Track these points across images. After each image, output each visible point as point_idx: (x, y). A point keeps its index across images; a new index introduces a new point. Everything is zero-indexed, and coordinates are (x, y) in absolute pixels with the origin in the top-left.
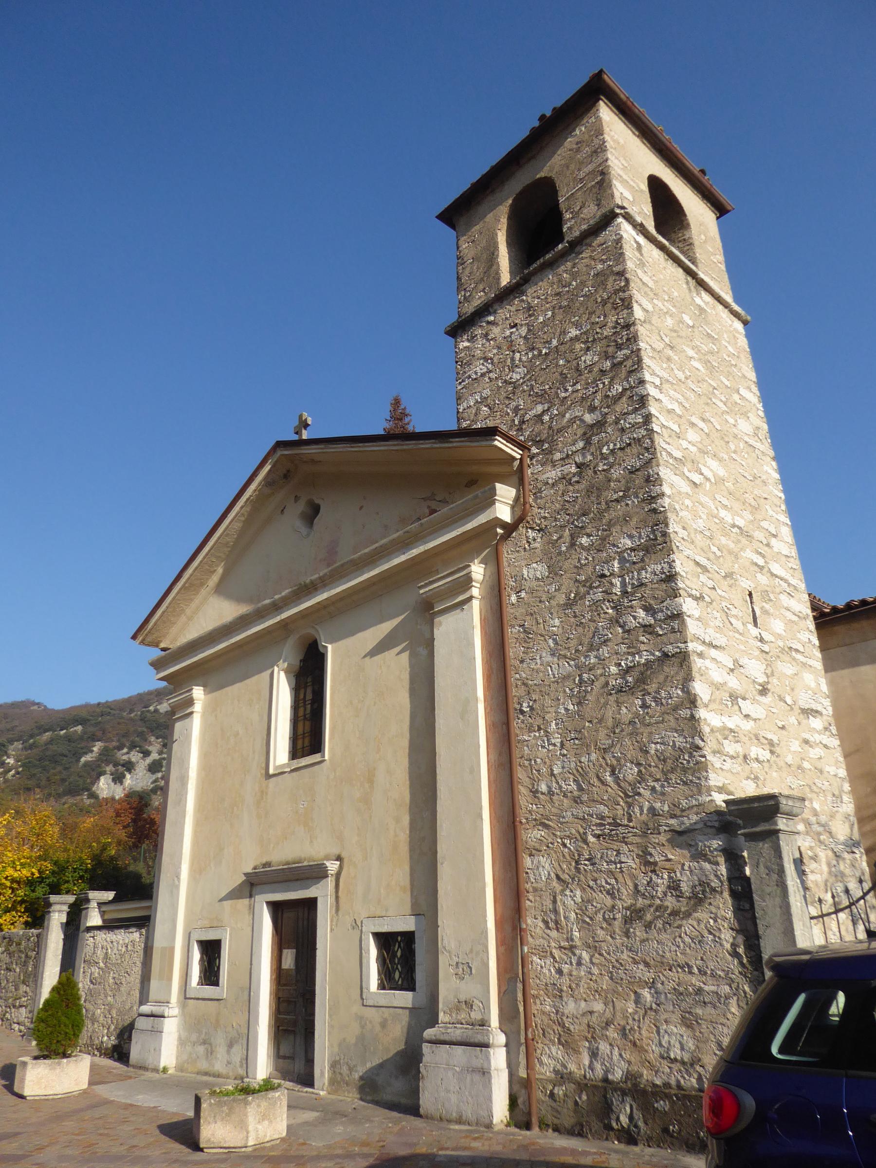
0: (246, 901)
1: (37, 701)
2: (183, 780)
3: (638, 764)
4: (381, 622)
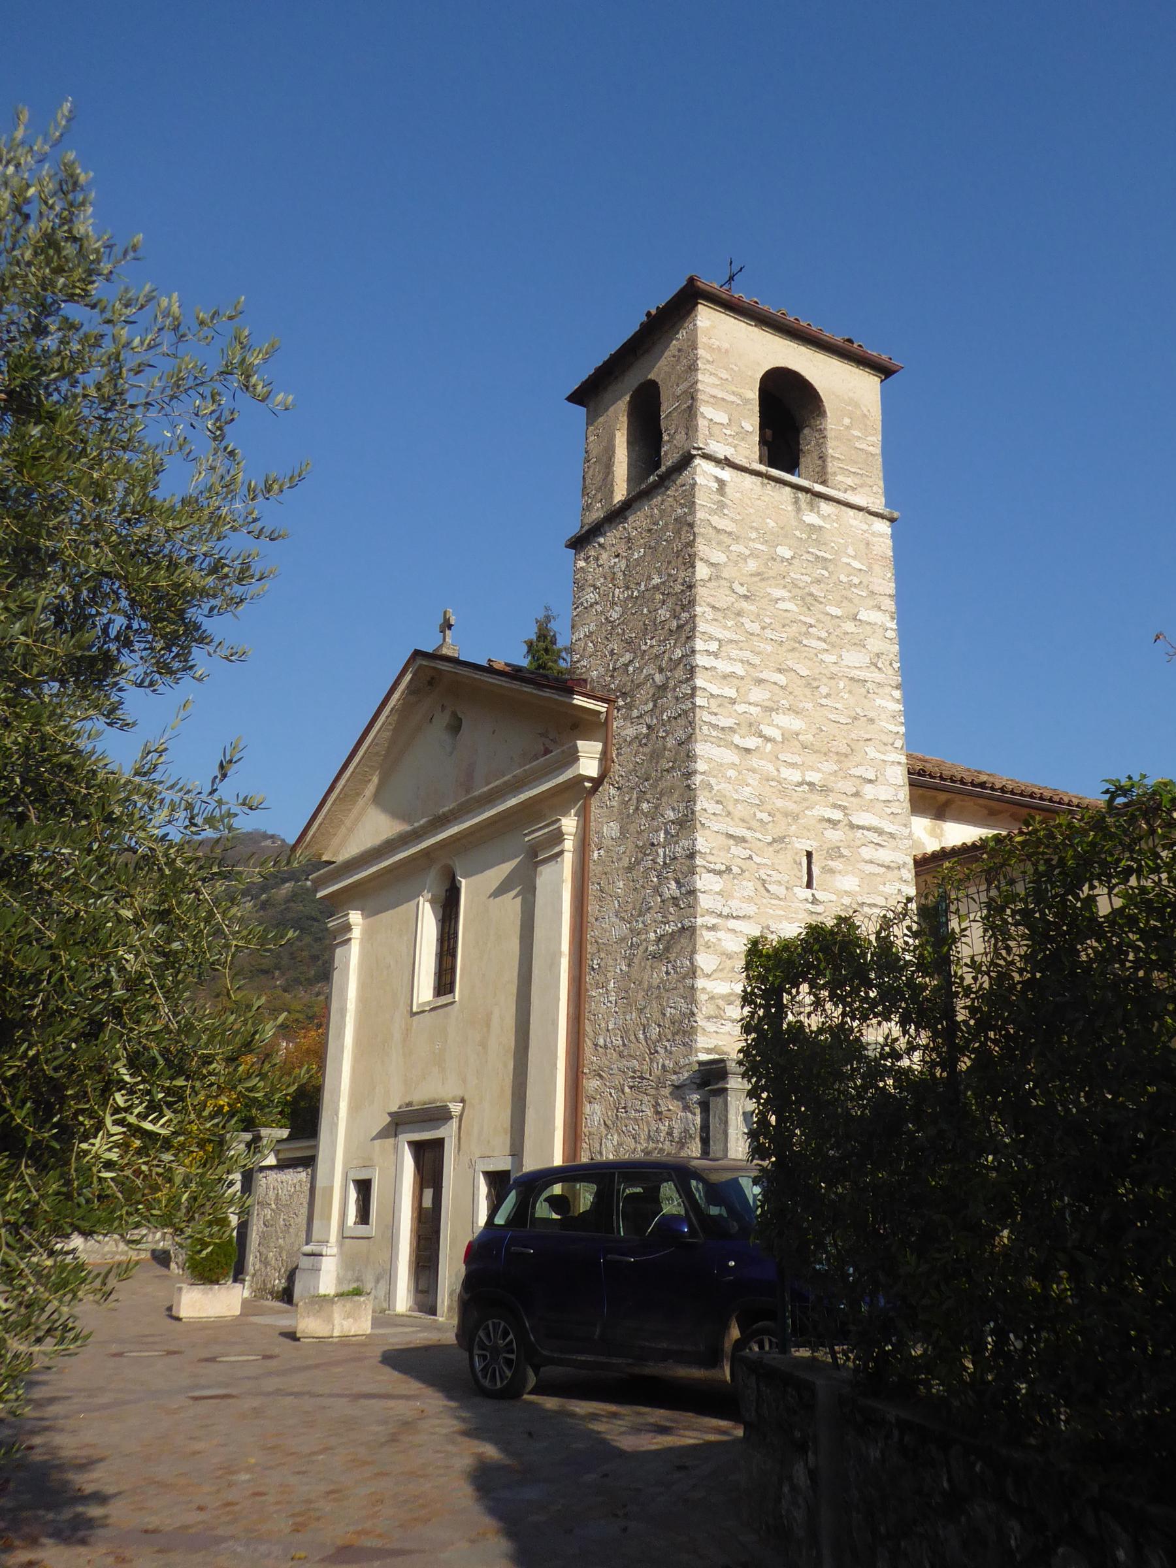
0: (391, 1141)
1: (270, 832)
2: (343, 1011)
3: (659, 1026)
4: (503, 862)
